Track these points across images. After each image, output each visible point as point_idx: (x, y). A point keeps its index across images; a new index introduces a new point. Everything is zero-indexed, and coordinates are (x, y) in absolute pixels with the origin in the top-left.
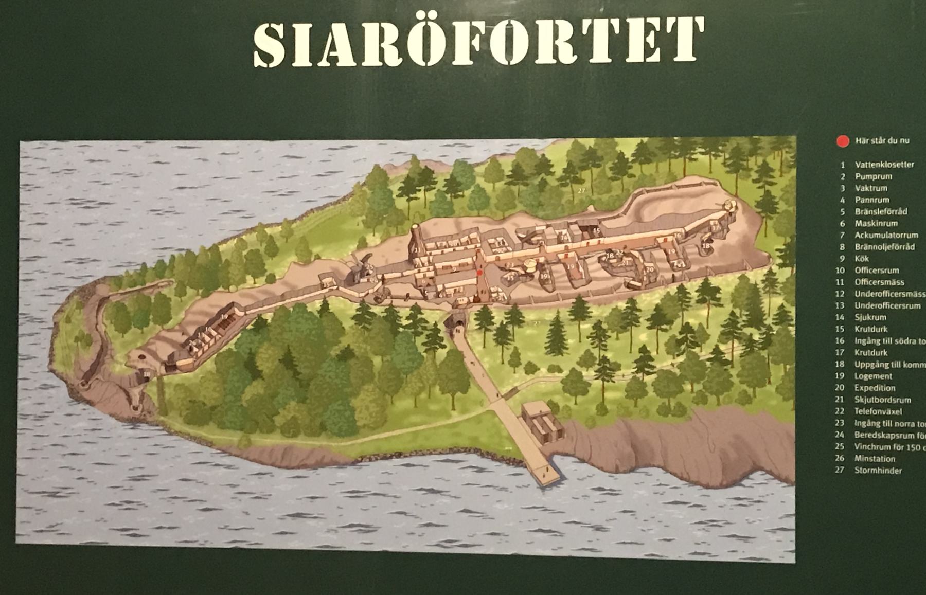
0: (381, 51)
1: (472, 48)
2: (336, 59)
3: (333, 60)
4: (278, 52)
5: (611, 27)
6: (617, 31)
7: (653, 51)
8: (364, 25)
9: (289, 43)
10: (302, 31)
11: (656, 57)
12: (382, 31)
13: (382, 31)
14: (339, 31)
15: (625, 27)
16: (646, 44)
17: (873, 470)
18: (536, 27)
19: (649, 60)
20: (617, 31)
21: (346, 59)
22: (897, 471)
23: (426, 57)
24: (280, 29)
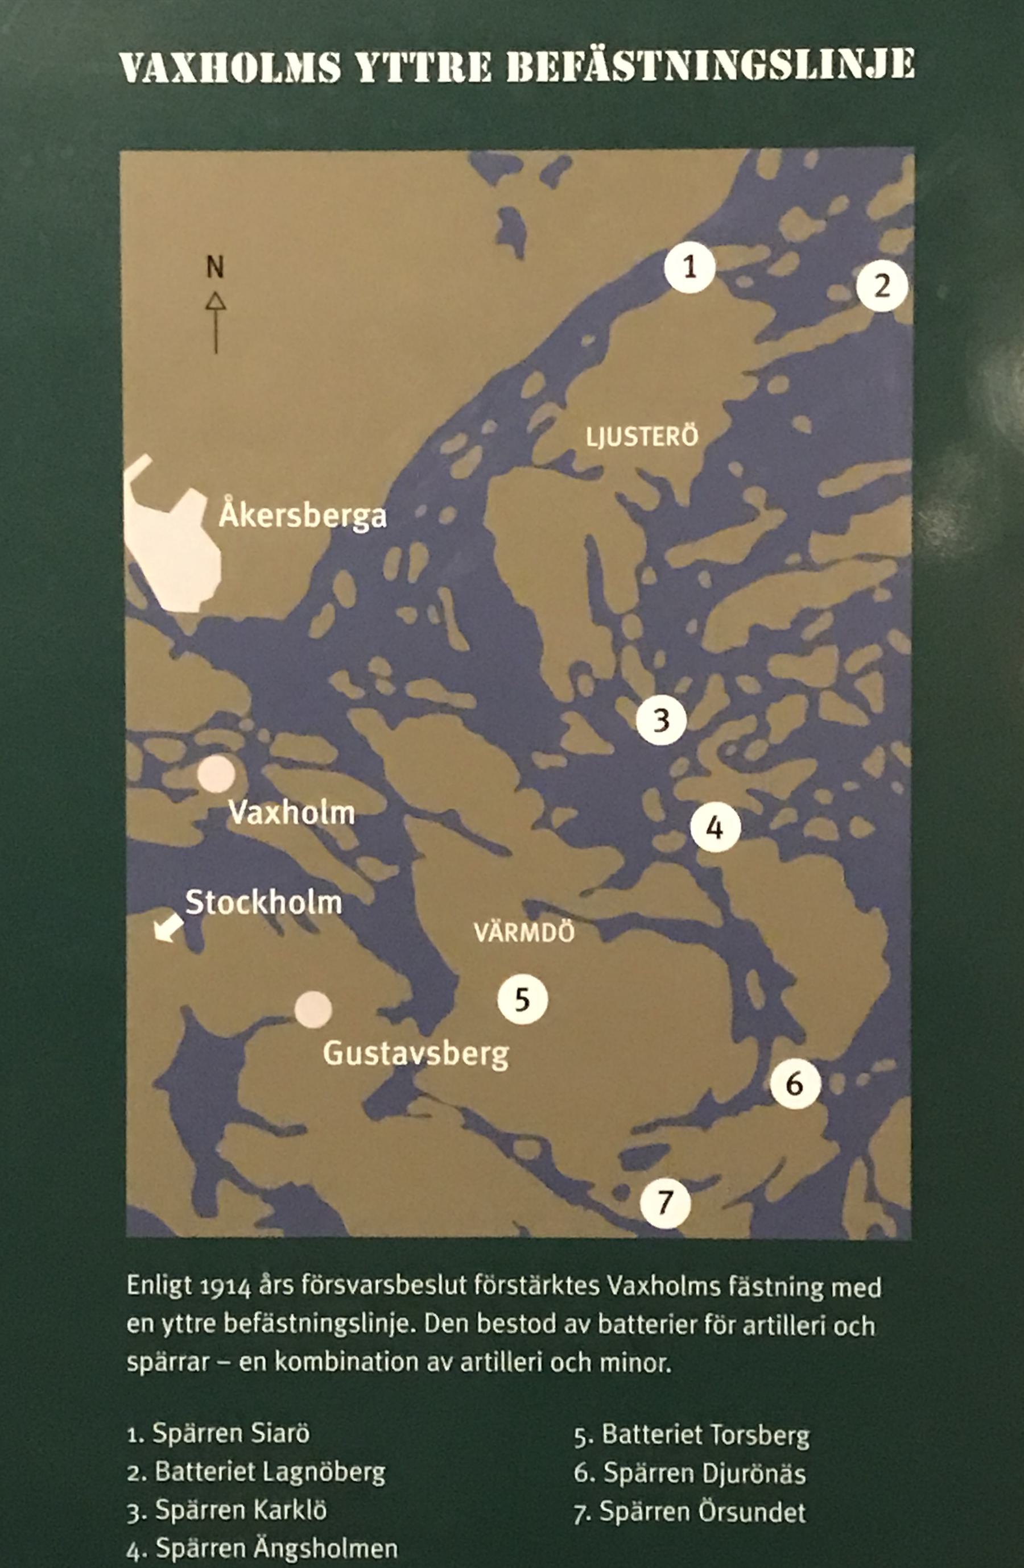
0: (521, 70)
1: (576, 70)
2: (596, 75)
3: (594, 76)
4: (787, 69)
5: (656, 56)
6: (660, 59)
7: (486, 74)
8: (875, 50)
9: (793, 61)
10: (803, 54)
11: (488, 79)
12: (521, 59)
13: (521, 59)
14: (157, 58)
15: (437, 58)
16: (550, 70)
17: (369, 1287)
18: (469, 57)
19: (484, 80)
20: (660, 59)
21: (162, 77)
22: (305, 1291)
23: (245, 76)
24: (788, 53)
